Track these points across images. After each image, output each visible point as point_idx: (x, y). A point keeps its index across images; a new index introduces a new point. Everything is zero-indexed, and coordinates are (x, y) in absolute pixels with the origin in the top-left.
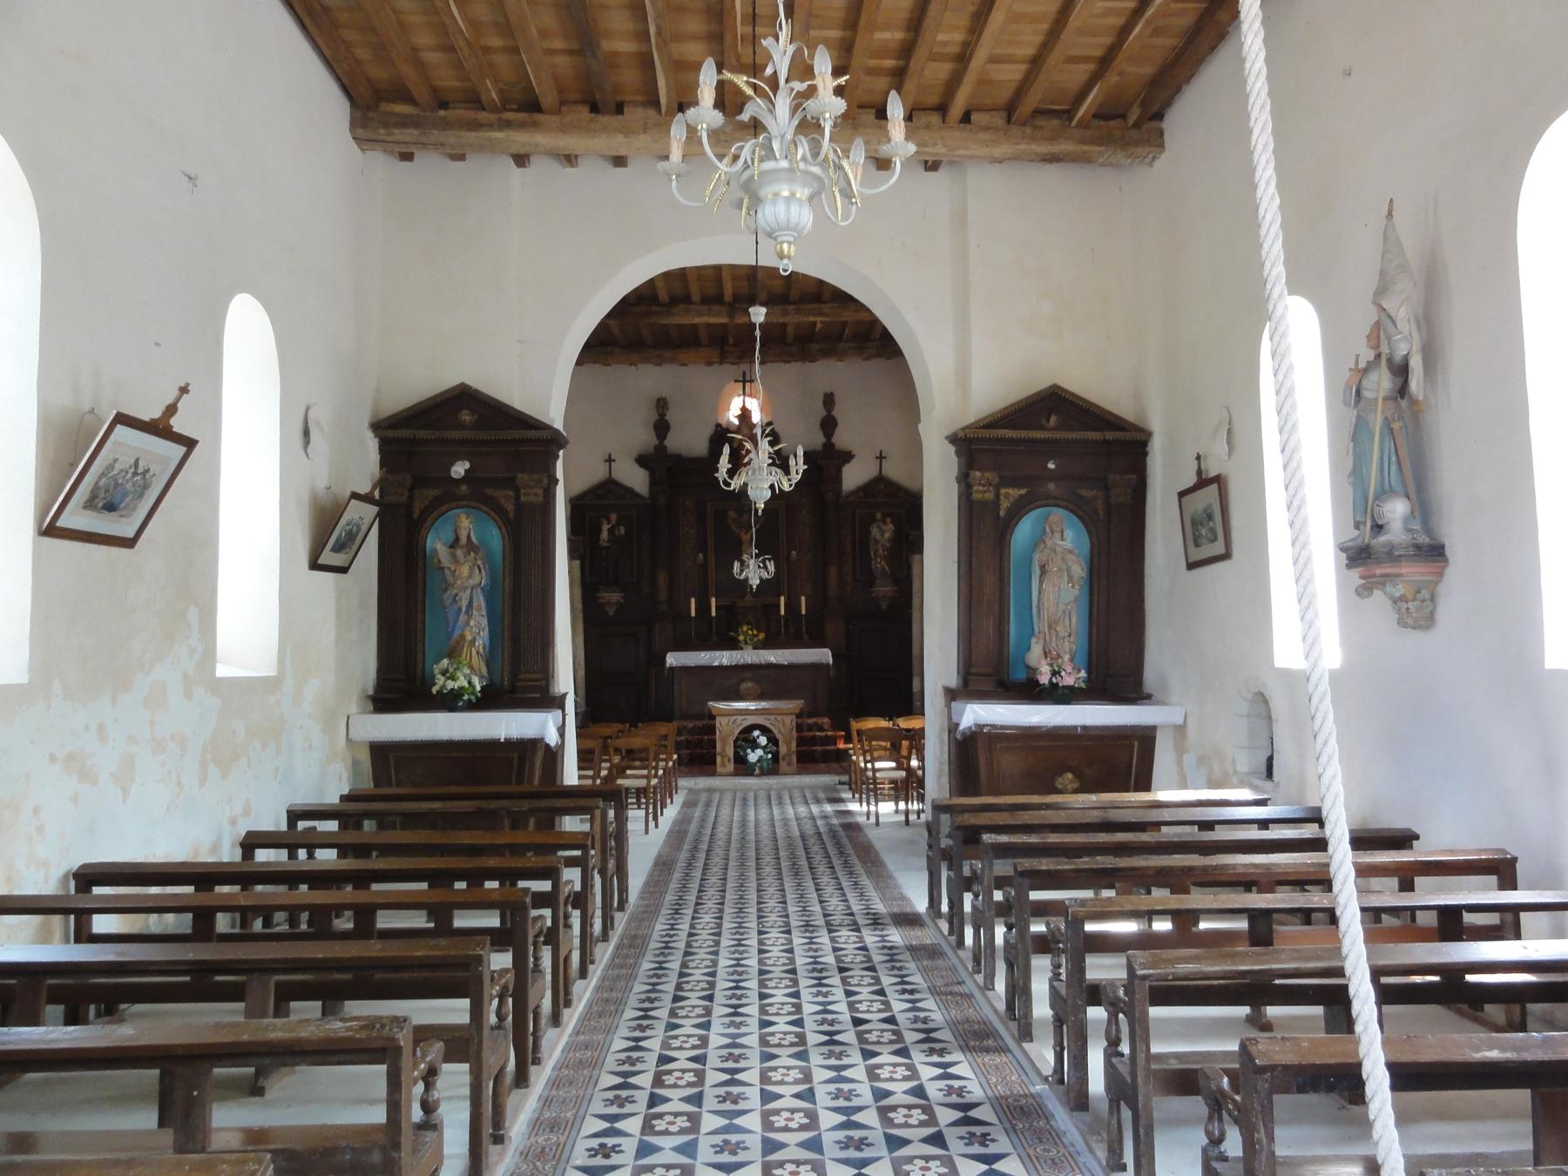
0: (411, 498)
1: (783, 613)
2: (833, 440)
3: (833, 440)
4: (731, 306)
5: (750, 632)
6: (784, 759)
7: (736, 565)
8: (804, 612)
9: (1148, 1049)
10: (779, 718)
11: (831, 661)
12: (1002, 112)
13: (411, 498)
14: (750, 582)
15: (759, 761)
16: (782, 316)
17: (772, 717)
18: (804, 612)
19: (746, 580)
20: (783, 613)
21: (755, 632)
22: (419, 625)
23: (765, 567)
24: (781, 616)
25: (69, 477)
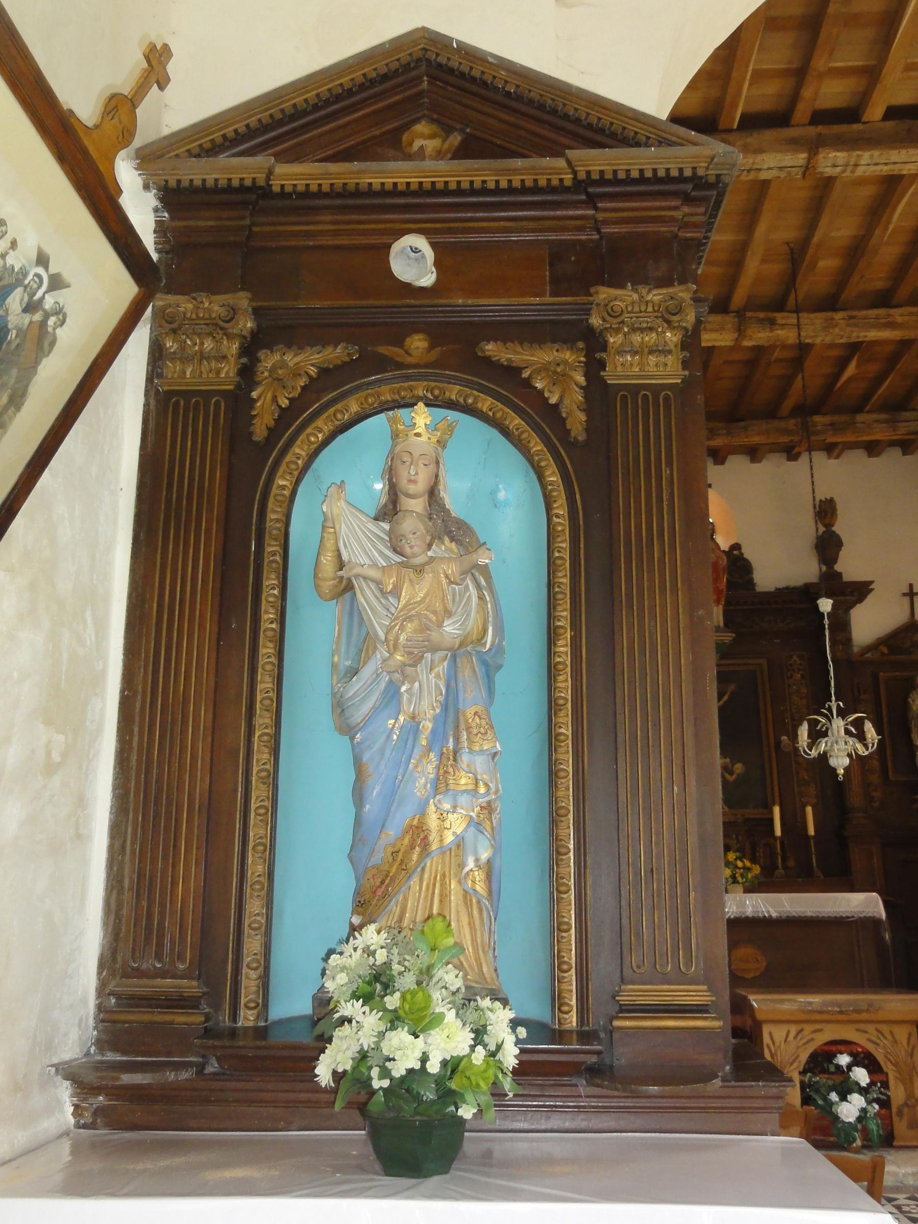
0: (247, 374)
1: (778, 832)
2: (838, 567)
3: (838, 567)
4: (740, 314)
5: (740, 864)
6: (900, 1114)
7: (803, 731)
8: (811, 831)
9: (66, 739)
10: (885, 1028)
11: (884, 916)
12: (798, 341)
13: (247, 374)
14: (833, 762)
15: (859, 1119)
16: (709, 439)
17: (871, 1028)
18: (811, 831)
19: (824, 757)
20: (778, 832)
21: (748, 864)
22: (258, 792)
23: (861, 737)
24: (775, 838)
25: (733, 1140)
